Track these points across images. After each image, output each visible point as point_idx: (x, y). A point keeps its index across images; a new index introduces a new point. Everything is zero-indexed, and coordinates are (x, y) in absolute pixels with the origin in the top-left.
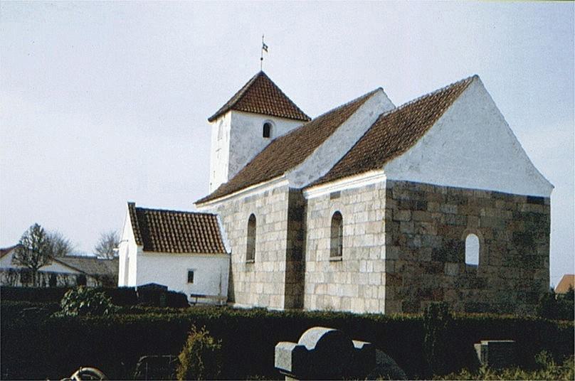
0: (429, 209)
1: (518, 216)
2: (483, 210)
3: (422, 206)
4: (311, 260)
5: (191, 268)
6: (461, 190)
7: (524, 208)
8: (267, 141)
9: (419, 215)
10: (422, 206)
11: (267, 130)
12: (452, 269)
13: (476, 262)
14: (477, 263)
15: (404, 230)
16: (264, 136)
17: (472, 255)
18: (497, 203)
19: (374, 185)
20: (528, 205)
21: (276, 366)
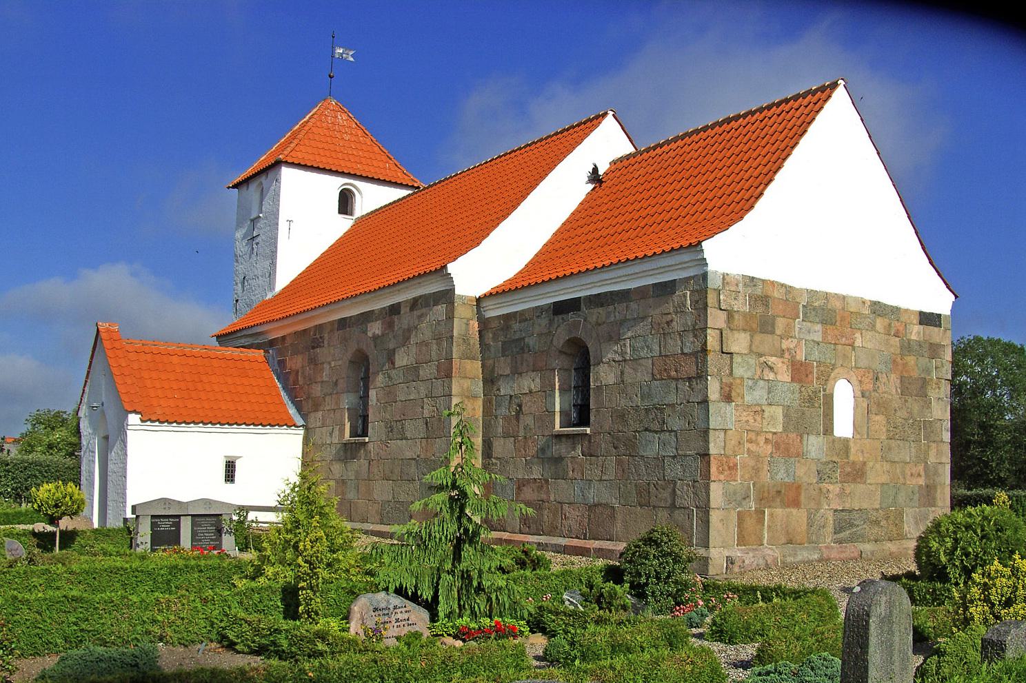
0: (778, 332)
1: (907, 347)
2: (858, 335)
3: (765, 326)
4: (506, 435)
5: (232, 453)
6: (827, 296)
7: (916, 332)
8: (344, 224)
9: (765, 342)
10: (765, 326)
11: (345, 202)
12: (814, 445)
13: (97, 527)
14: (850, 436)
15: (739, 371)
16: (341, 212)
17: (843, 426)
18: (880, 323)
19: (580, 297)
20: (922, 327)
21: (717, 555)
